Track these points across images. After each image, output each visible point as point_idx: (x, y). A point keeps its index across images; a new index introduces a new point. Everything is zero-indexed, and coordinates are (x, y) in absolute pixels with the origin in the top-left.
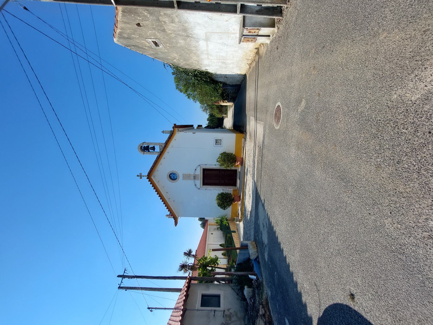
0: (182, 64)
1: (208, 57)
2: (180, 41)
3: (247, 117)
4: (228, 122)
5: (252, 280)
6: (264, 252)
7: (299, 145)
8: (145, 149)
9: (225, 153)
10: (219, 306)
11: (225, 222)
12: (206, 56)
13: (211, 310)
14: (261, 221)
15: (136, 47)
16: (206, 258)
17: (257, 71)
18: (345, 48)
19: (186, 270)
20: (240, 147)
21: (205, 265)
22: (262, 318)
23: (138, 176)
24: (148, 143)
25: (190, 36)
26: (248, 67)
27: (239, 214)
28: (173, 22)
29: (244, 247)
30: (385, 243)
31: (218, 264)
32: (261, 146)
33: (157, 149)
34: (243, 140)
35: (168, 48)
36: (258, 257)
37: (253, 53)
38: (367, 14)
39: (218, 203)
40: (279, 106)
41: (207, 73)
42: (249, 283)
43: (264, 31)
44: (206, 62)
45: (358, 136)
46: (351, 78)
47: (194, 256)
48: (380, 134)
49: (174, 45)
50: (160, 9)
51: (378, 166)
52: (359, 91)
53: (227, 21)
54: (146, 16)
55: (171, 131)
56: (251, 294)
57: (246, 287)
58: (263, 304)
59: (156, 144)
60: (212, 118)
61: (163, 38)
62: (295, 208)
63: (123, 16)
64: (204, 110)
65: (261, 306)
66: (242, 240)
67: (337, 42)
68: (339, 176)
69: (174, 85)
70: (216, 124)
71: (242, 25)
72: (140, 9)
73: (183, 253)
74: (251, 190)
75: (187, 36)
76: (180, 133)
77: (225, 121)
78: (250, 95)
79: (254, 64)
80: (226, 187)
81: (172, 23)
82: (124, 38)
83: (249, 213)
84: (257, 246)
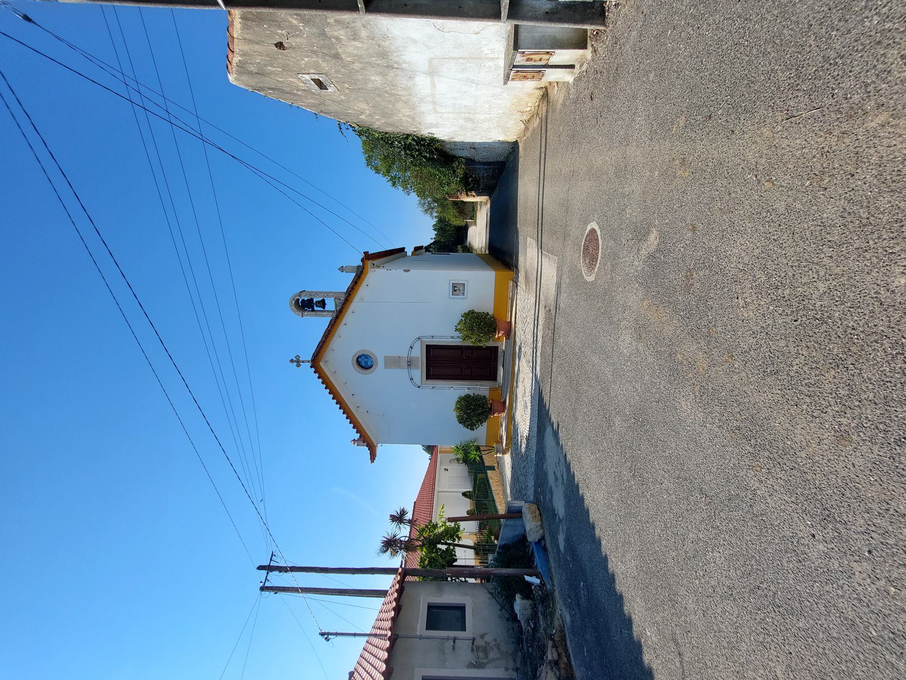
0: (378, 123)
1: (435, 109)
2: (373, 78)
3: (521, 238)
4: (478, 235)
5: (530, 584)
6: (557, 532)
7: (640, 330)
8: (306, 305)
9: (472, 312)
10: (463, 629)
11: (473, 455)
12: (431, 107)
13: (448, 639)
14: (550, 465)
15: (277, 92)
16: (435, 526)
17: (544, 140)
18: (766, 132)
19: (394, 550)
20: (505, 298)
21: (433, 541)
22: (552, 669)
23: (292, 361)
24: (310, 292)
25: (396, 66)
26: (523, 126)
27: (501, 438)
28: (355, 37)
29: (514, 514)
30: (851, 615)
31: (459, 538)
32: (552, 308)
33: (331, 305)
34: (511, 283)
35: (347, 91)
36: (543, 538)
37: (534, 100)
38: (833, 54)
39: (458, 417)
40: (593, 231)
41: (433, 140)
42: (527, 590)
43: (562, 56)
44: (430, 119)
45: (793, 351)
46: (781, 207)
47: (411, 522)
48: (850, 360)
49: (360, 86)
50: (325, 13)
51: (842, 436)
52: (801, 244)
53: (477, 33)
54: (296, 28)
55: (358, 267)
56: (529, 612)
57: (518, 597)
58: (553, 640)
59: (328, 294)
60: (442, 227)
61: (336, 72)
62: (629, 464)
63: (245, 27)
64: (426, 211)
65: (550, 643)
66: (509, 499)
67: (746, 111)
68: (739, 428)
69: (362, 159)
70: (450, 241)
71: (512, 44)
72: (282, 14)
73: (389, 517)
74: (528, 393)
75: (388, 66)
76: (378, 270)
77: (472, 231)
78: (527, 188)
79: (536, 122)
80: (476, 382)
81: (354, 39)
82: (250, 73)
83: (524, 441)
84: (540, 514)
